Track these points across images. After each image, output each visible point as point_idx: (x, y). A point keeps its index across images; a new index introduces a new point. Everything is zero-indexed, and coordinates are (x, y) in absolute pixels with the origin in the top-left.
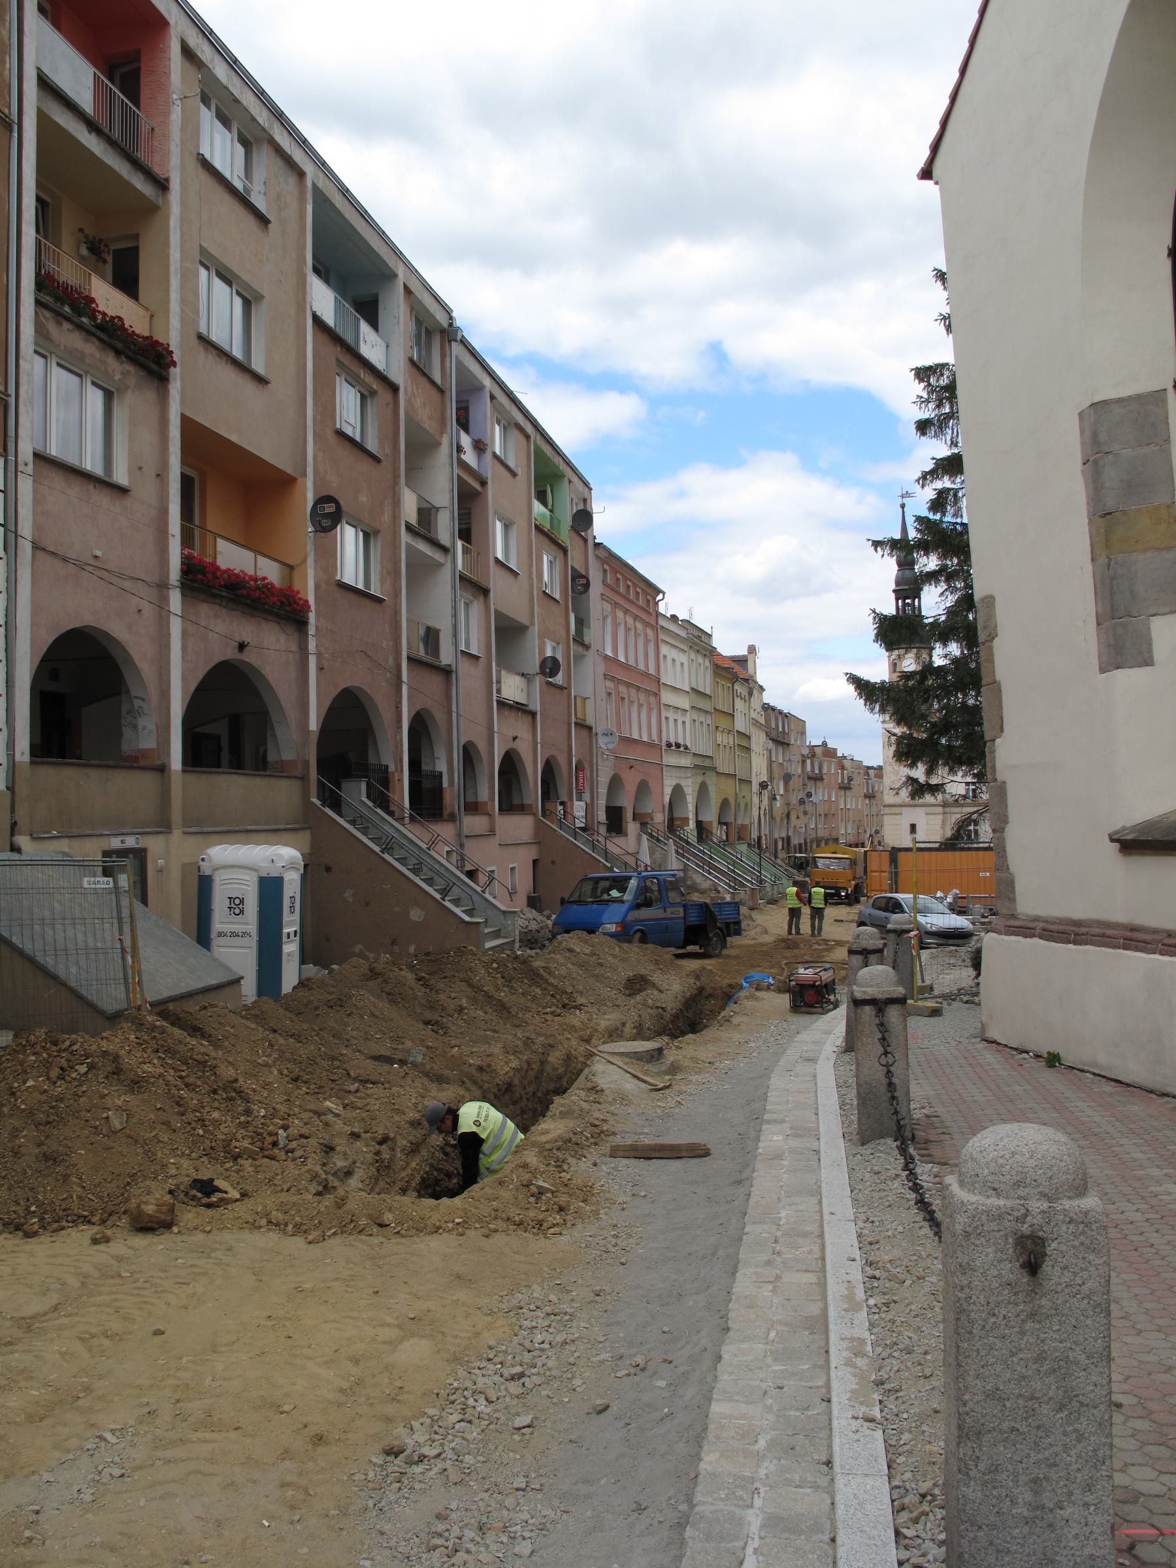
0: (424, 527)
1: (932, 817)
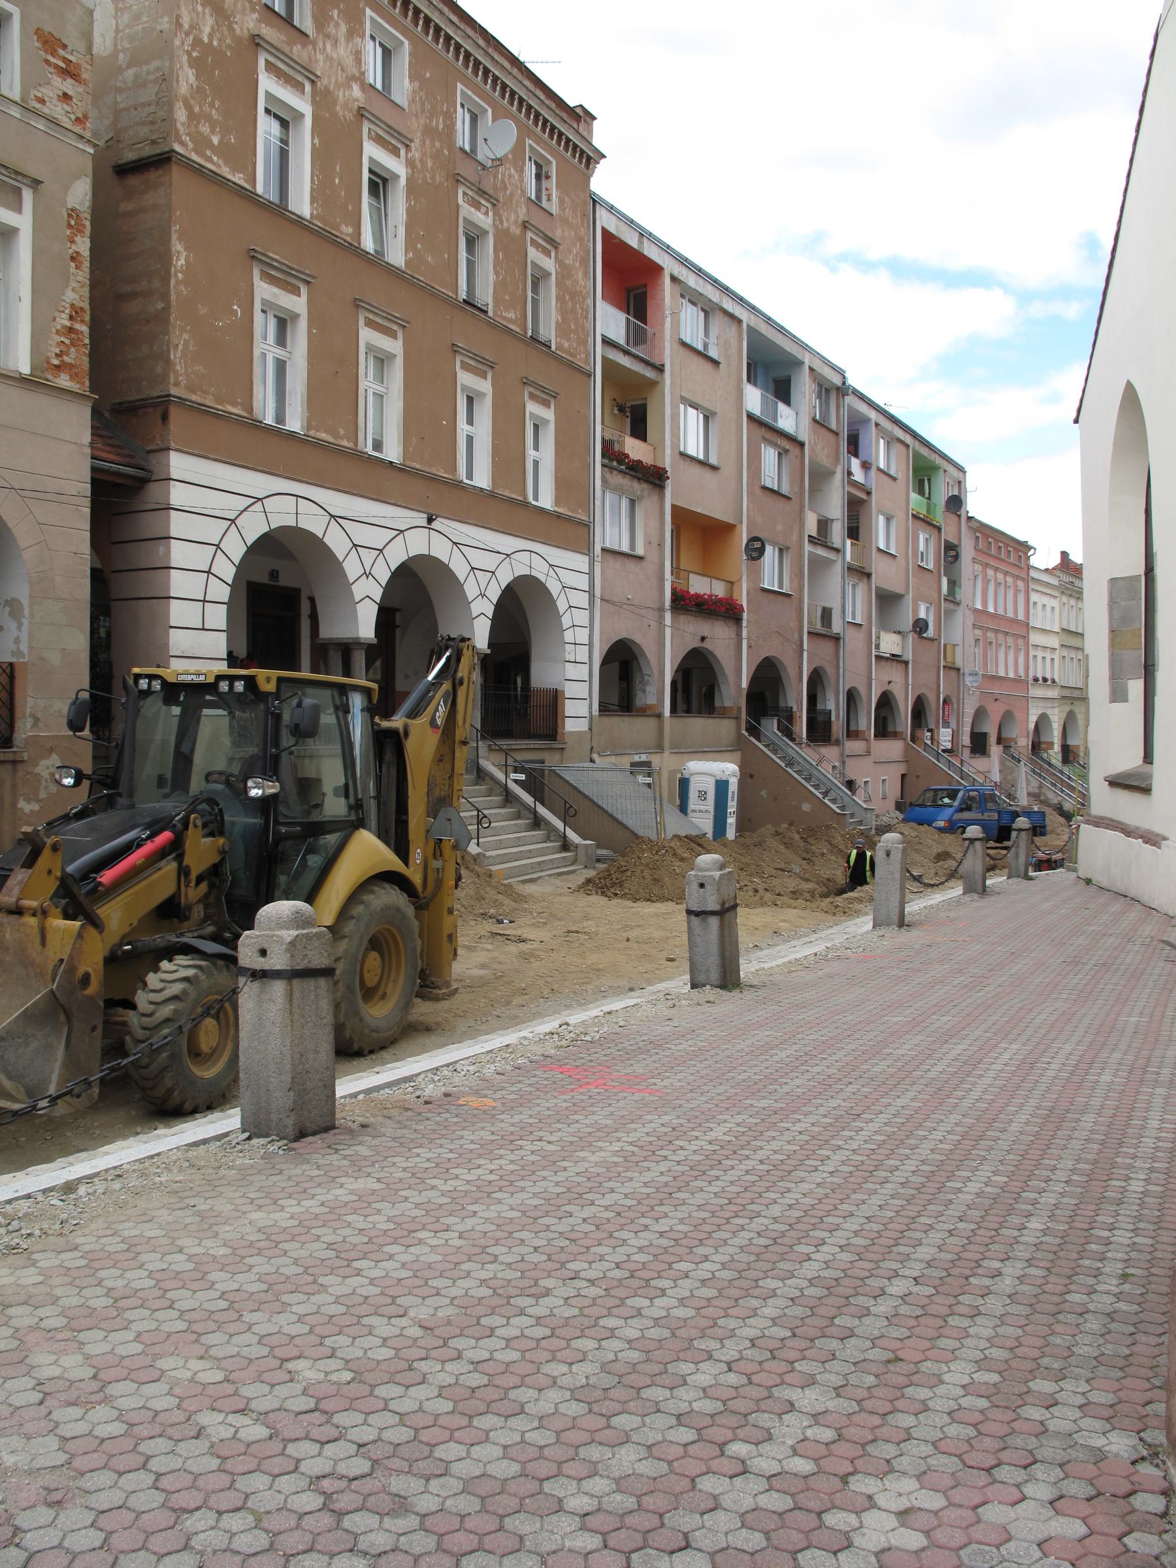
0: (821, 538)
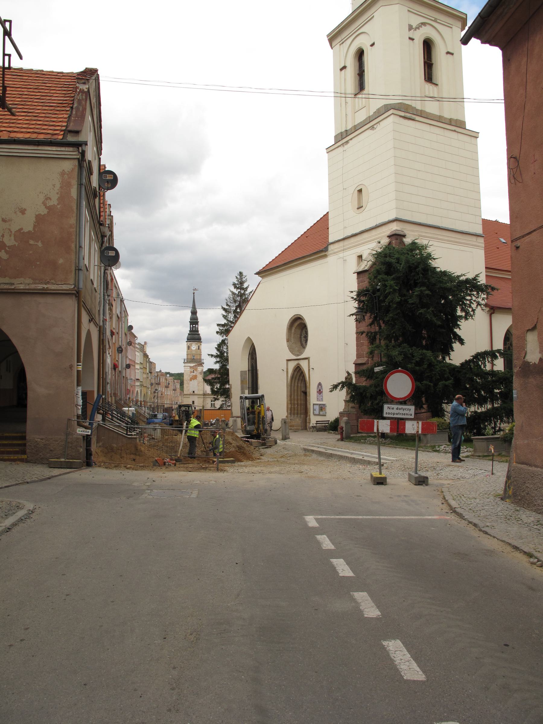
1: (200, 399)
